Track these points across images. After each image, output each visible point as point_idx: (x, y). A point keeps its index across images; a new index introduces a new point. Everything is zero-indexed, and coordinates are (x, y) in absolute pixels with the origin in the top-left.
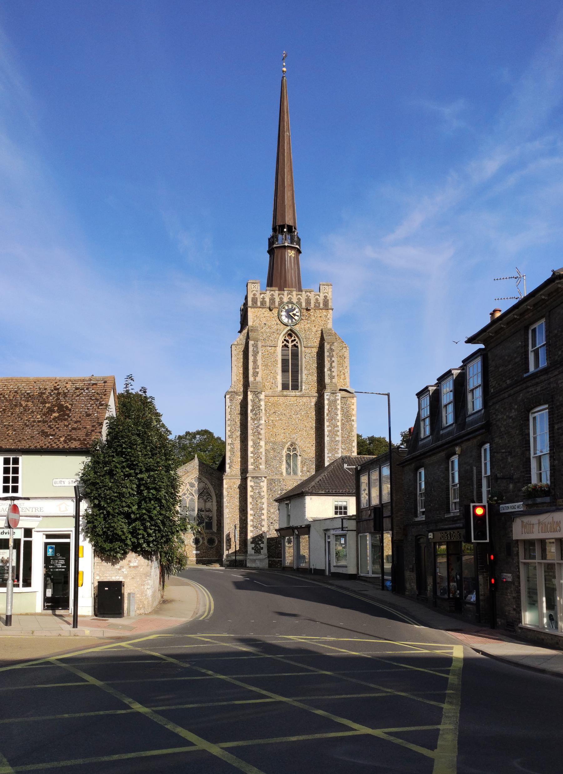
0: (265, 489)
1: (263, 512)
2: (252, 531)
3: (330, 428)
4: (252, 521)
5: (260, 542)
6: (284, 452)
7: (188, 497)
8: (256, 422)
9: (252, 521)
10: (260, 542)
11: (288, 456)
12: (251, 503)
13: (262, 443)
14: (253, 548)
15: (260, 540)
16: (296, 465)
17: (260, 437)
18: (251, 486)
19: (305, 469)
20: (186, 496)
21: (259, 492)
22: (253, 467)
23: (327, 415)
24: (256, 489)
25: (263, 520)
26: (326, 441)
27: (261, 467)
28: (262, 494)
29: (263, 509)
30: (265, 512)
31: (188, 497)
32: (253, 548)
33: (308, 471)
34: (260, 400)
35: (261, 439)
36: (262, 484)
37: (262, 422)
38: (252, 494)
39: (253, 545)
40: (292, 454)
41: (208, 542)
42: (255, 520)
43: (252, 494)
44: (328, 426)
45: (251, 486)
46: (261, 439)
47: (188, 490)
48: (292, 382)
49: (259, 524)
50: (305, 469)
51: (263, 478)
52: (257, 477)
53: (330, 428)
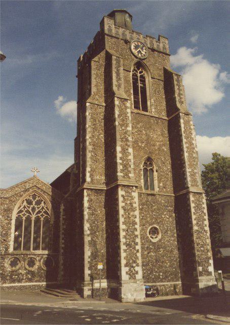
0: (136, 200)
1: (136, 226)
2: (125, 251)
3: (187, 145)
4: (125, 237)
5: (134, 265)
6: (142, 166)
7: (24, 215)
8: (123, 128)
9: (125, 237)
10: (134, 265)
11: (145, 170)
12: (123, 216)
13: (130, 150)
14: (89, 275)
15: (135, 262)
16: (152, 181)
17: (128, 144)
18: (123, 196)
19: (161, 185)
20: (23, 213)
21: (131, 203)
22: (122, 174)
23: (184, 133)
24: (128, 199)
25: (137, 236)
26: (185, 156)
27: (130, 175)
28: (134, 205)
29: (136, 224)
30: (137, 226)
31: (24, 215)
32: (127, 273)
33: (164, 188)
34: (126, 108)
35: (129, 146)
36: (133, 194)
37: (129, 129)
38: (124, 204)
39: (127, 269)
40: (149, 169)
41: (34, 264)
42: (128, 237)
43: (124, 204)
44: (186, 143)
45: (123, 196)
46: (129, 146)
47: (25, 207)
48: (141, 101)
49: (133, 241)
50: (161, 185)
51: (134, 188)
52: (128, 186)
53: (187, 145)
